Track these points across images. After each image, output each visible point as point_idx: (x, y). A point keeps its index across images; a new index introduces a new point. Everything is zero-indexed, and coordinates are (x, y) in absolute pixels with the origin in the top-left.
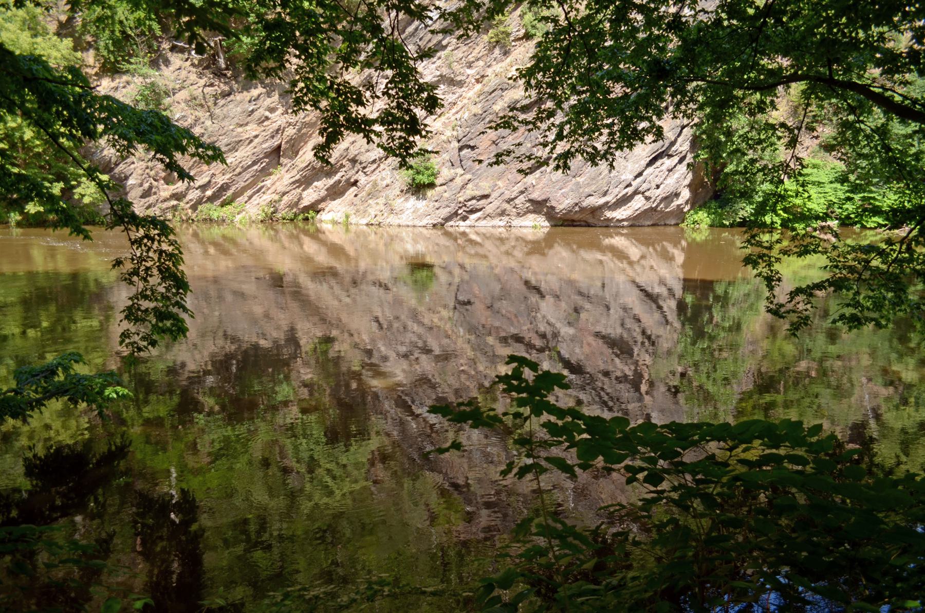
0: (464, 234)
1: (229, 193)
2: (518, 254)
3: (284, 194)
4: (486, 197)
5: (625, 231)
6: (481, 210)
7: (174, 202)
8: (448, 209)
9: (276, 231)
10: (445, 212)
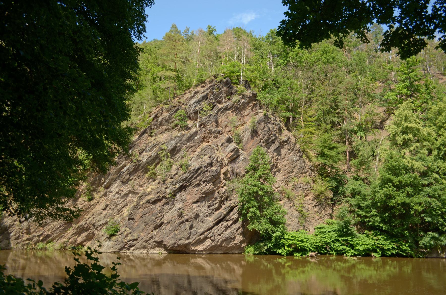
0: (128, 256)
1: (50, 238)
2: (150, 266)
3: (70, 239)
4: (136, 240)
5: (204, 256)
6: (134, 246)
7: (27, 242)
8: (120, 245)
9: (66, 254)
10: (119, 246)
